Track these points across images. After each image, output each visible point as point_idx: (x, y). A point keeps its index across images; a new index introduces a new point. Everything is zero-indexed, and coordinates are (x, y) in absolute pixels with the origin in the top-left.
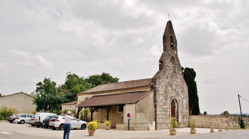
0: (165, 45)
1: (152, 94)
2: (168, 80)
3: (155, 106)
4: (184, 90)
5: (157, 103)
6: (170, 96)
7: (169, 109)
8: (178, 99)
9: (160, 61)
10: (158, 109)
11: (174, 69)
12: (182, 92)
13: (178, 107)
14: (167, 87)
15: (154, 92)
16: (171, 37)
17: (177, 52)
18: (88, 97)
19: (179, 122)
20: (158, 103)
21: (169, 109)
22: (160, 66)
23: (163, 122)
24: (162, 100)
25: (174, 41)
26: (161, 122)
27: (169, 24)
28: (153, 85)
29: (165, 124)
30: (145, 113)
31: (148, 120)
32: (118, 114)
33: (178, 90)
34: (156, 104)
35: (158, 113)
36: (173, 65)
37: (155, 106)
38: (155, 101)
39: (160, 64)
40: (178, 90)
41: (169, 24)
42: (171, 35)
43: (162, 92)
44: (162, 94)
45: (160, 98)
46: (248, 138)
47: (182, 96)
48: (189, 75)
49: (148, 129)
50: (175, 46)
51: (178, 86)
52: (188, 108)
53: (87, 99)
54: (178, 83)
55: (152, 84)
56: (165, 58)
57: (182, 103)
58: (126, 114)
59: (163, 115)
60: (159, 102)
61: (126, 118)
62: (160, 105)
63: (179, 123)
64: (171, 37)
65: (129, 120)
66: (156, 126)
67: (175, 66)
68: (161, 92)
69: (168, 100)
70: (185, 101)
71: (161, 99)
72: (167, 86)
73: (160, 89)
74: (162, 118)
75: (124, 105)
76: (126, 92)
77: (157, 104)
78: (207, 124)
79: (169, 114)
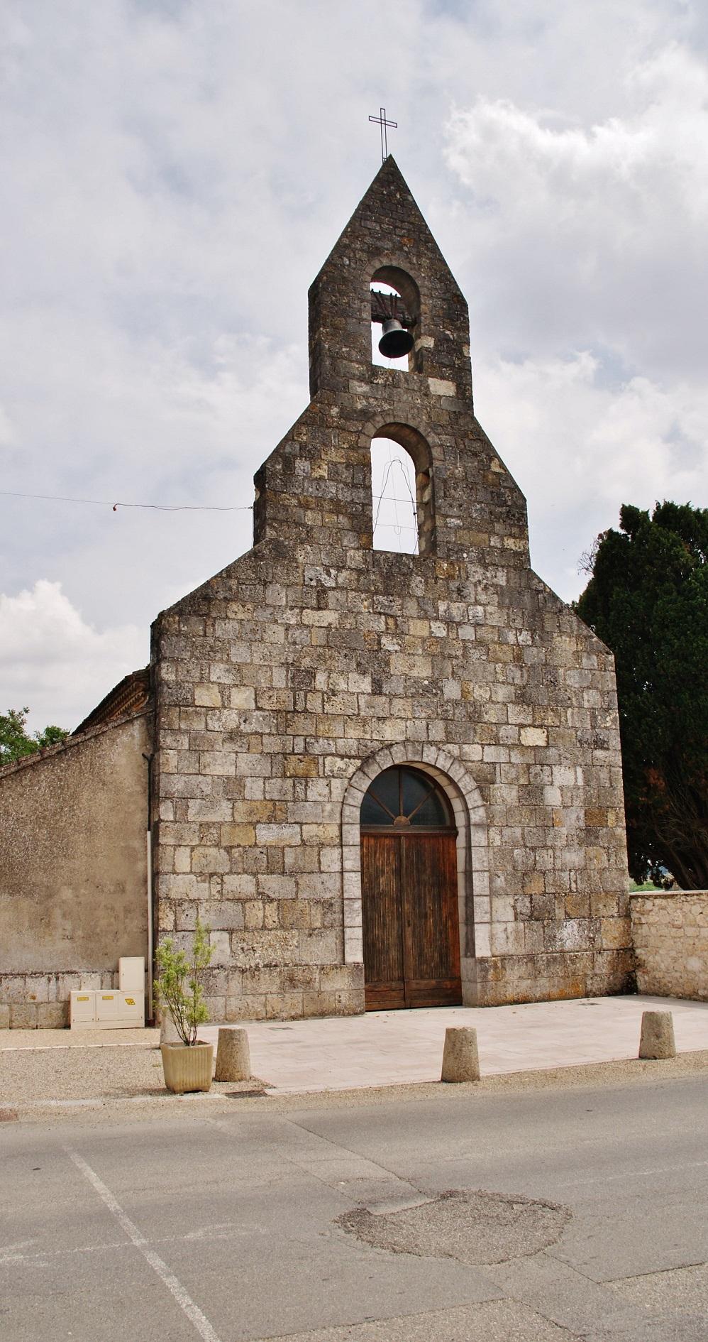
2: (329, 617)
4: (554, 683)
6: (350, 745)
7: (330, 858)
8: (461, 760)
12: (522, 698)
13: (467, 810)
14: (301, 678)
29: (265, 976)
30: (29, 894)
31: (67, 944)
33: (465, 693)
37: (153, 795)
46: (686, 1291)
47: (534, 737)
49: (63, 1022)
50: (441, 340)
51: (475, 654)
52: (622, 833)
54: (467, 633)
62: (205, 826)
63: (483, 961)
66: (151, 998)
69: (323, 782)
70: (563, 779)
74: (231, 931)
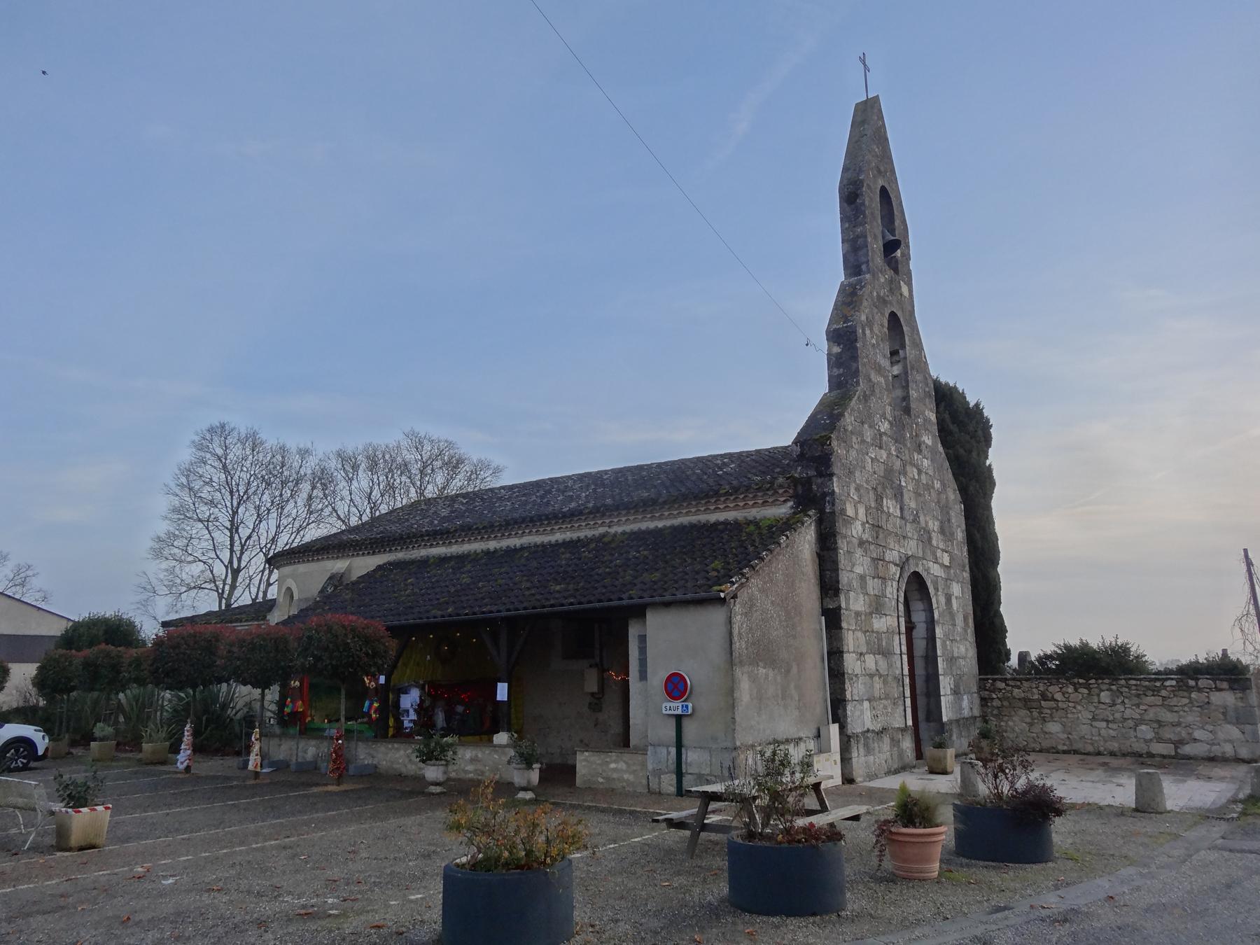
0: (858, 237)
1: (806, 540)
3: (833, 619)
5: (842, 597)
9: (835, 336)
10: (852, 640)
11: (899, 393)
14: (879, 499)
15: (820, 522)
16: (884, 192)
17: (911, 291)
18: (349, 569)
19: (945, 719)
20: (847, 600)
21: (897, 638)
22: (835, 362)
23: (878, 727)
24: (862, 578)
25: (897, 223)
26: (869, 724)
27: (868, 121)
28: (808, 481)
32: (1180, 816)
34: (839, 608)
35: (851, 663)
36: (896, 370)
37: (833, 619)
38: (829, 585)
39: (836, 350)
40: (927, 523)
41: (868, 121)
42: (881, 182)
43: (863, 524)
44: (862, 543)
45: (854, 566)
48: (962, 433)
53: (336, 580)
55: (804, 474)
56: (863, 318)
57: (949, 599)
58: (657, 678)
59: (871, 676)
60: (852, 594)
61: (648, 708)
64: (884, 192)
65: (679, 719)
67: (906, 373)
68: (858, 523)
71: (859, 570)
72: (879, 489)
73: (850, 511)
75: (639, 612)
76: (612, 530)
77: (843, 605)
78: (1103, 732)
79: (898, 672)
